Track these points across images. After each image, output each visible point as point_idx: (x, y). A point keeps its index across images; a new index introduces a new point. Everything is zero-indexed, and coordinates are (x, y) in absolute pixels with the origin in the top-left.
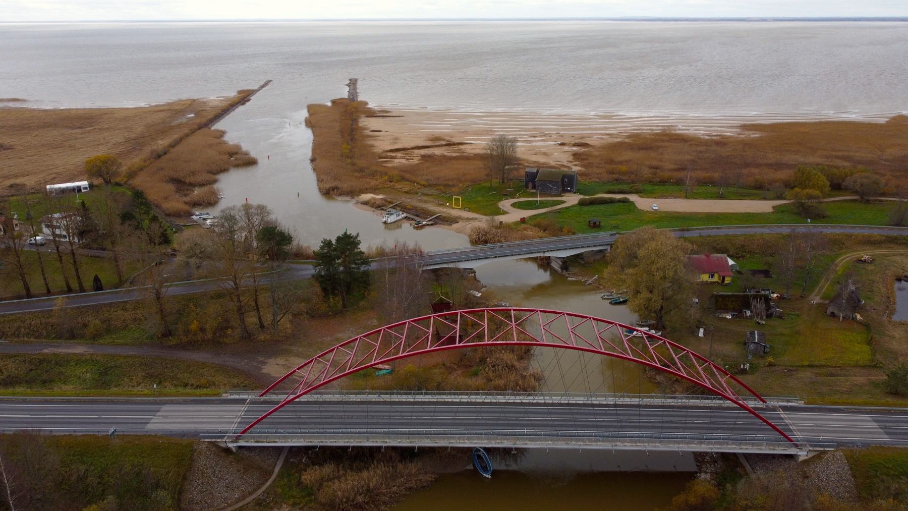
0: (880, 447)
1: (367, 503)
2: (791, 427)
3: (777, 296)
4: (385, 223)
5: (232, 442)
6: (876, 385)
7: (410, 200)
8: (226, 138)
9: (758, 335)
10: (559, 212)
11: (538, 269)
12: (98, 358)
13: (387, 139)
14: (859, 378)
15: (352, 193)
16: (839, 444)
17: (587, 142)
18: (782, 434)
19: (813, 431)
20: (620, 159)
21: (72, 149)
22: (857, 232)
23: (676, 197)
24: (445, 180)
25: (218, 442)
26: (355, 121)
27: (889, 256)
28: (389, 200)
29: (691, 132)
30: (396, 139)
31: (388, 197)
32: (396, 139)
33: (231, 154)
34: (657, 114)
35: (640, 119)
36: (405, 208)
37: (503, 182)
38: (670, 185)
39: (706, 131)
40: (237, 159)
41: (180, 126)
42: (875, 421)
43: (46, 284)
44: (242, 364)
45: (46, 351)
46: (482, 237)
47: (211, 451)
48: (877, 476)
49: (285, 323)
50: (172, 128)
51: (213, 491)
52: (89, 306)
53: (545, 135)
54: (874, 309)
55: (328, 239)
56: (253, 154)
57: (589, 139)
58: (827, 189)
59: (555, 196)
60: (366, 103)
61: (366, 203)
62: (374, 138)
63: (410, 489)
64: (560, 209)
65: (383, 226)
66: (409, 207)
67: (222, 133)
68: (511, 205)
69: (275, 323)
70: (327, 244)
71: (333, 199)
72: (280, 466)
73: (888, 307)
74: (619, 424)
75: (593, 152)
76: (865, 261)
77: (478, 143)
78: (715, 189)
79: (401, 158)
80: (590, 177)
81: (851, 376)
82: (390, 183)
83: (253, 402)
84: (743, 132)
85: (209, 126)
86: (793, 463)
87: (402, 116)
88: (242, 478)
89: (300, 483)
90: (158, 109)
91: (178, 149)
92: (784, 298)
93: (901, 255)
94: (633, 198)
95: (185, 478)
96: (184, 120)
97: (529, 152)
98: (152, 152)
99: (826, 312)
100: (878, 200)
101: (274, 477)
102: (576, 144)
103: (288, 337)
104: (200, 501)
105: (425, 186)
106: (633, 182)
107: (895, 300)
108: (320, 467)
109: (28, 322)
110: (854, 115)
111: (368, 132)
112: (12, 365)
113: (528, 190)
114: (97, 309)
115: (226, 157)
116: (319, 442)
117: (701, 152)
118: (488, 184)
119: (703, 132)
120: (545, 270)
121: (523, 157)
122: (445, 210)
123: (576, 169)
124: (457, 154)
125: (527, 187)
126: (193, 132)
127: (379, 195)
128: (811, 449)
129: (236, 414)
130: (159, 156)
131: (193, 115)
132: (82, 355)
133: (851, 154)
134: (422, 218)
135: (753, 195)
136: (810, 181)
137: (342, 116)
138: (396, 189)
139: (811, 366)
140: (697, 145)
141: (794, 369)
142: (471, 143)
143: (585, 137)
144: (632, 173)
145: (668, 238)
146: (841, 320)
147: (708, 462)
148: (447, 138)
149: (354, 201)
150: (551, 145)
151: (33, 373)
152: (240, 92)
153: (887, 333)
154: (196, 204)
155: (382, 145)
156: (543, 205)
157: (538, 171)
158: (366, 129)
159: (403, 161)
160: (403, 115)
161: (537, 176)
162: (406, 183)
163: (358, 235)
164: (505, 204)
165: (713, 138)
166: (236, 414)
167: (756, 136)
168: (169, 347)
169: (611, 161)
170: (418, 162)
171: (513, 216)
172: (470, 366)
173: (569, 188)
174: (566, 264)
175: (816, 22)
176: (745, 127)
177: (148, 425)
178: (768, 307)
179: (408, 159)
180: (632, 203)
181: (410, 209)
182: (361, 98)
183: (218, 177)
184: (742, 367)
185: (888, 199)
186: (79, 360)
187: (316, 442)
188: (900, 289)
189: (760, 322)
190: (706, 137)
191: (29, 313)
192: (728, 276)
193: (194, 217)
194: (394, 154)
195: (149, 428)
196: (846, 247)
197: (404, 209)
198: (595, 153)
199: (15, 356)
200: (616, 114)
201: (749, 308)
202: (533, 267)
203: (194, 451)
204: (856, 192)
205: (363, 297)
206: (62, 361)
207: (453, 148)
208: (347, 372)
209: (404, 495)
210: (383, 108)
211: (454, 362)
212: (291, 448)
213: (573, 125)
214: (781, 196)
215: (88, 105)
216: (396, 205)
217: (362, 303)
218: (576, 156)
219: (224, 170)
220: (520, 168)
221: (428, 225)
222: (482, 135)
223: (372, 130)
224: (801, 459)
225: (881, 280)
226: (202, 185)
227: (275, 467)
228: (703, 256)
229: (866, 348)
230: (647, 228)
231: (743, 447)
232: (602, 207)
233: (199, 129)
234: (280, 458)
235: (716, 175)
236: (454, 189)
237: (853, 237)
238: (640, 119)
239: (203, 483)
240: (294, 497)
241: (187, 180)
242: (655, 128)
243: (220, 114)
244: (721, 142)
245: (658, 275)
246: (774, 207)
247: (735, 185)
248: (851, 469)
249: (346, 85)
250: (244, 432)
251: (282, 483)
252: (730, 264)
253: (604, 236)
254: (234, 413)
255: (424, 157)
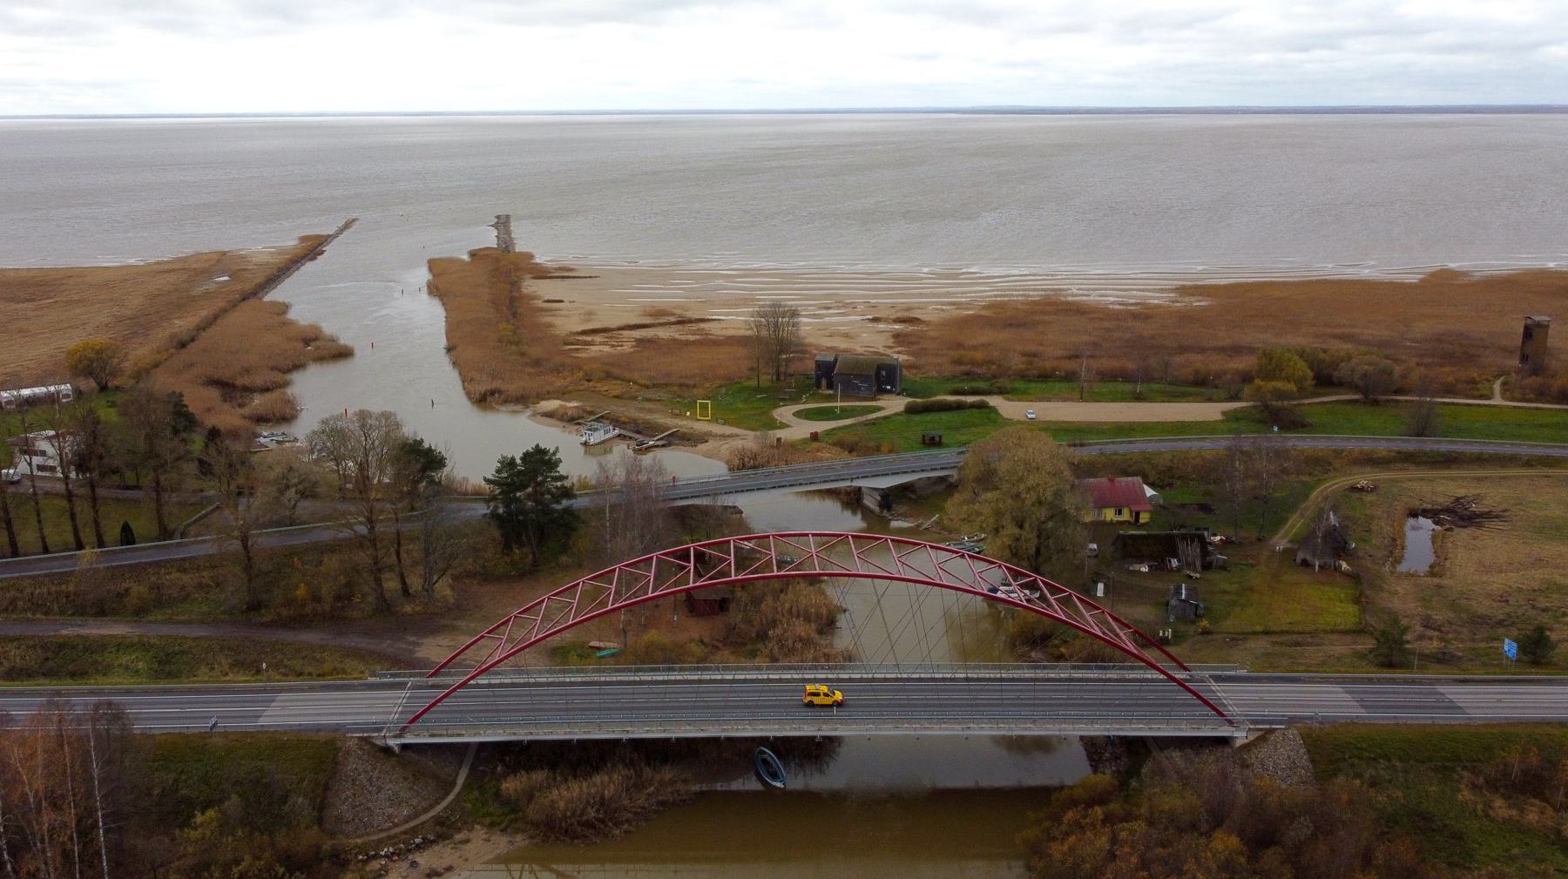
0: (1352, 723)
1: (602, 821)
2: (1225, 702)
3: (1221, 540)
4: (585, 444)
5: (395, 737)
6: (1361, 656)
7: (624, 409)
8: (292, 315)
9: (1186, 590)
10: (874, 424)
11: (843, 510)
12: (152, 641)
13: (574, 314)
14: (1338, 647)
15: (523, 400)
16: (1292, 721)
17: (919, 317)
18: (1214, 709)
19: (1259, 705)
20: (974, 342)
21: (24, 334)
22: (1350, 445)
23: (1065, 400)
24: (681, 377)
25: (373, 737)
26: (515, 285)
27: (1401, 482)
28: (589, 409)
29: (1094, 298)
30: (590, 314)
31: (586, 404)
32: (590, 313)
33: (307, 341)
34: (1033, 271)
35: (1007, 279)
36: (617, 421)
37: (778, 379)
38: (1055, 381)
39: (1117, 296)
40: (318, 348)
41: (207, 295)
42: (1347, 692)
43: (43, 538)
44: (386, 646)
45: (64, 632)
46: (749, 462)
47: (364, 749)
48: (1345, 759)
49: (444, 588)
50: (194, 299)
51: (370, 805)
52: (125, 566)
53: (845, 305)
54: (1370, 556)
55: (509, 456)
56: (345, 340)
57: (919, 311)
58: (1309, 383)
59: (865, 399)
60: (531, 256)
61: (549, 415)
62: (549, 313)
63: (662, 803)
64: (877, 419)
65: (582, 449)
66: (623, 419)
67: (284, 308)
68: (794, 414)
69: (428, 588)
70: (508, 464)
71: (492, 409)
72: (465, 776)
73: (1391, 552)
74: (973, 702)
75: (927, 331)
76: (1362, 489)
77: (732, 319)
78: (1128, 387)
79: (601, 344)
80: (923, 371)
81: (1326, 645)
82: (586, 383)
83: (415, 687)
84: (1179, 299)
85: (260, 295)
86: (1228, 750)
87: (596, 277)
88: (411, 788)
89: (497, 794)
90: (162, 267)
91: (212, 331)
92: (1232, 542)
93: (1421, 479)
94: (994, 401)
95: (327, 788)
96: (211, 286)
97: (819, 332)
98: (172, 337)
99: (1295, 560)
100: (1392, 400)
101: (457, 789)
102: (898, 318)
103: (449, 609)
104: (353, 820)
105: (647, 387)
106: (994, 377)
107: (1404, 542)
108: (527, 772)
109: (28, 591)
110: (1368, 271)
111: (539, 303)
112: (15, 653)
113: (821, 391)
114: (137, 571)
115: (301, 345)
116: (526, 734)
117: (1108, 330)
118: (753, 383)
119: (1111, 299)
120: (854, 513)
121: (809, 340)
122: (684, 423)
123: (902, 358)
124: (698, 337)
125: (818, 386)
126: (234, 305)
127: (570, 402)
128: (1252, 727)
129: (396, 701)
130: (183, 345)
131: (226, 278)
132: (124, 637)
133: (1357, 330)
134: (647, 435)
135: (1191, 394)
136: (1282, 370)
137: (493, 277)
138: (599, 392)
139: (1266, 633)
140: (1101, 319)
141: (1241, 637)
142: (719, 320)
143: (912, 309)
144: (993, 363)
145: (1045, 448)
146: (1317, 570)
147: (1107, 760)
148: (678, 312)
149: (529, 412)
150: (857, 321)
151: (51, 664)
152: (304, 239)
153: (1387, 587)
154: (261, 419)
155: (567, 324)
156: (845, 413)
157: (836, 360)
158: (535, 298)
159: (606, 349)
160: (597, 275)
161: (834, 367)
162: (615, 382)
163: (557, 449)
164: (785, 413)
165: (1131, 308)
166: (396, 701)
167: (1201, 304)
168: (262, 624)
169: (960, 346)
170: (632, 350)
171: (800, 430)
172: (745, 644)
173: (889, 387)
174: (889, 499)
175: (1316, 115)
176: (1183, 291)
177: (261, 719)
178: (1205, 553)
179: (613, 346)
180: (993, 410)
181: (624, 423)
182: (520, 247)
183: (288, 377)
184: (1161, 634)
185: (1408, 398)
186: (122, 645)
187: (523, 735)
188: (1414, 528)
189: (1192, 575)
190: (1117, 307)
191: (29, 577)
192: (1145, 511)
193: (262, 440)
194: (589, 338)
195: (262, 722)
196: (1334, 469)
197: (616, 422)
198: (931, 333)
199: (17, 639)
200: (964, 270)
201: (1175, 555)
202: (832, 506)
203: (338, 749)
204: (1356, 388)
205: (565, 549)
206: (101, 645)
207: (688, 327)
208: (570, 622)
209: (655, 812)
210: (562, 264)
211: (717, 637)
212: (483, 746)
213: (893, 289)
214: (1237, 395)
215: (50, 263)
216: (602, 417)
217: (564, 559)
218: (897, 336)
219: (298, 366)
220: (806, 358)
221: (657, 446)
222: (737, 306)
223: (546, 299)
224: (1238, 743)
225: (1385, 515)
226: (266, 390)
227: (457, 776)
228: (1104, 480)
229: (1352, 609)
230: (1011, 430)
231: (1153, 726)
232: (945, 416)
233: (244, 299)
234: (463, 765)
235: (1131, 366)
236: (695, 391)
237: (1345, 453)
238: (1007, 279)
239: (354, 795)
240: (490, 815)
241: (239, 382)
242: (1031, 293)
243: (275, 276)
244: (1143, 314)
245: (1030, 498)
246: (1224, 413)
247: (1162, 379)
248: (1309, 751)
249: (492, 226)
250: (413, 721)
251: (472, 797)
252: (1148, 495)
253: (946, 456)
254: (391, 701)
255: (640, 342)
